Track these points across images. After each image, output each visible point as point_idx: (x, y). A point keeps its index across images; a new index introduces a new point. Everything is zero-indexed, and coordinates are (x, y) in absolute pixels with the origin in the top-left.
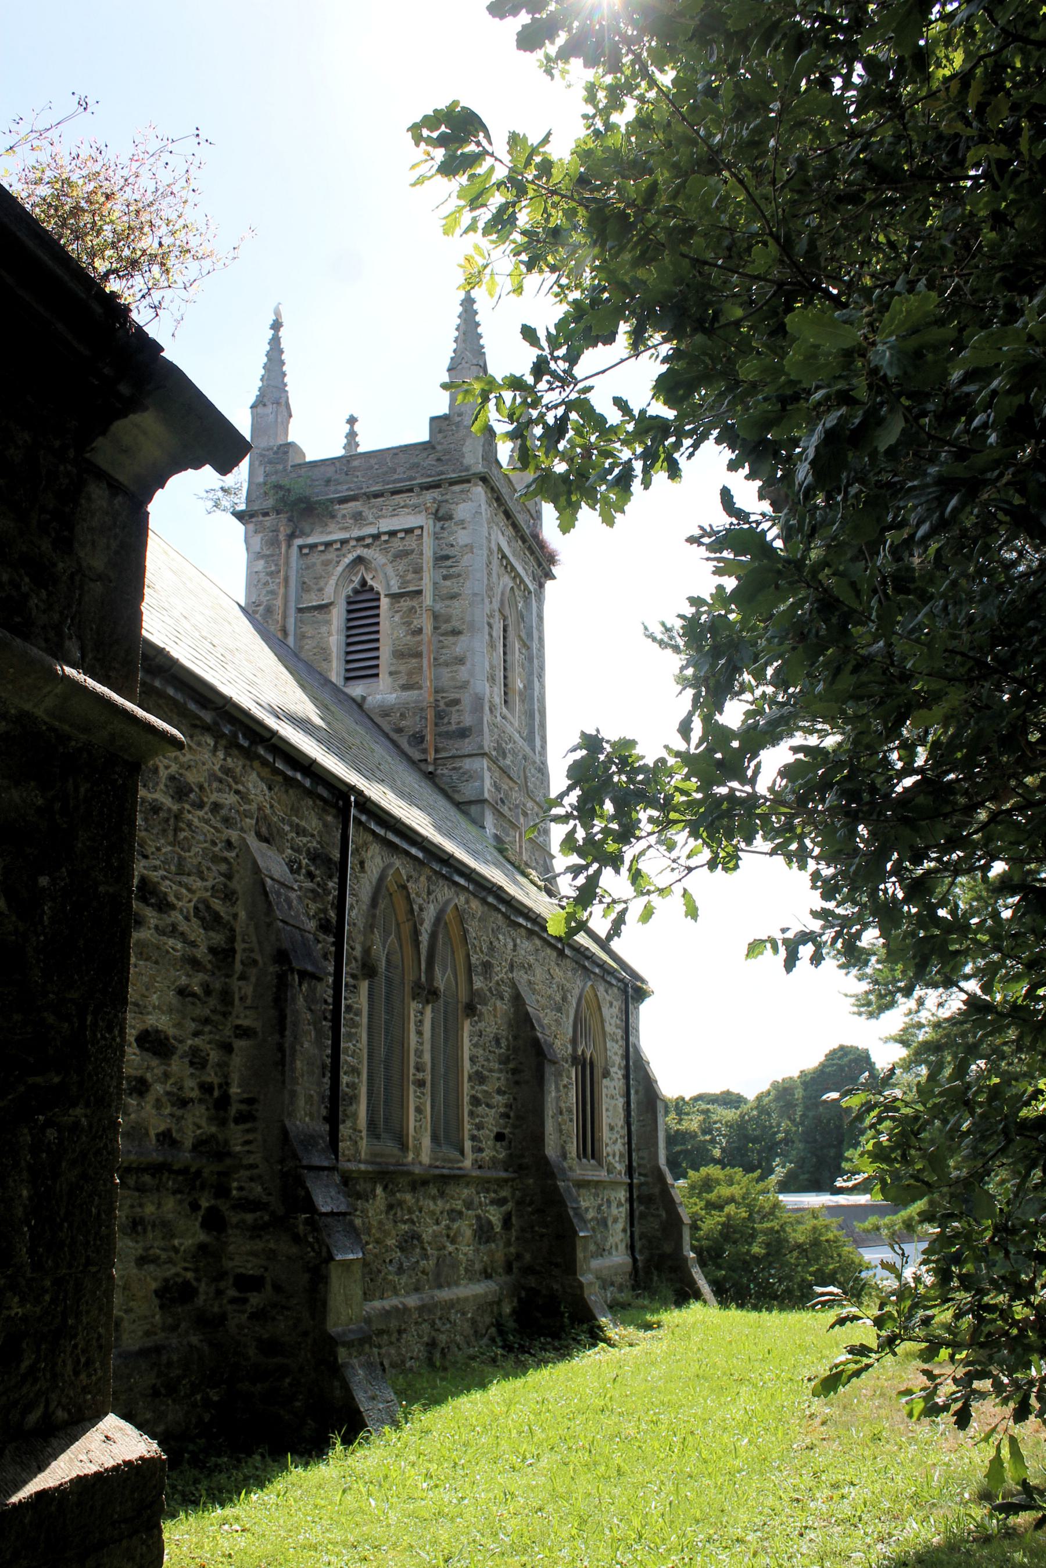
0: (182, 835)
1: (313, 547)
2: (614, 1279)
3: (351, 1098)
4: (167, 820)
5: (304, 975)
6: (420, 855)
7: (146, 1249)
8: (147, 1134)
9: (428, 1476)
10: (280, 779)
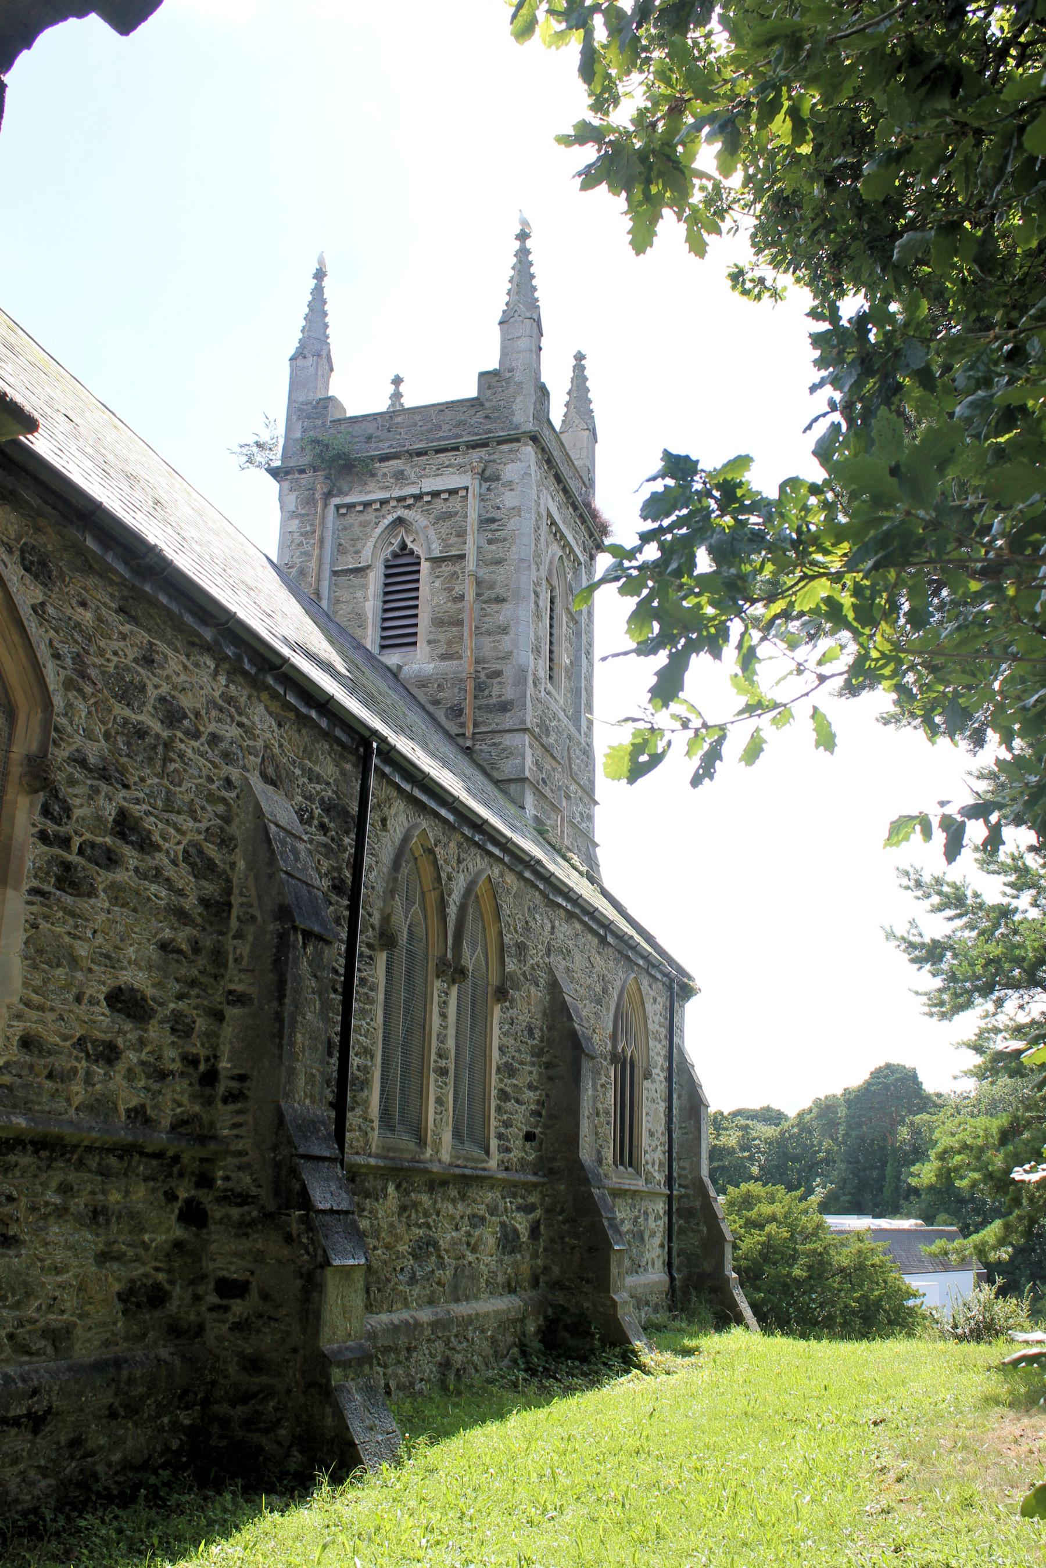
0: (172, 767)
1: (350, 506)
2: (649, 1298)
3: (362, 1083)
4: (154, 747)
5: (308, 935)
6: (451, 818)
7: (108, 1244)
8: (115, 1109)
9: (429, 1529)
10: (292, 715)
